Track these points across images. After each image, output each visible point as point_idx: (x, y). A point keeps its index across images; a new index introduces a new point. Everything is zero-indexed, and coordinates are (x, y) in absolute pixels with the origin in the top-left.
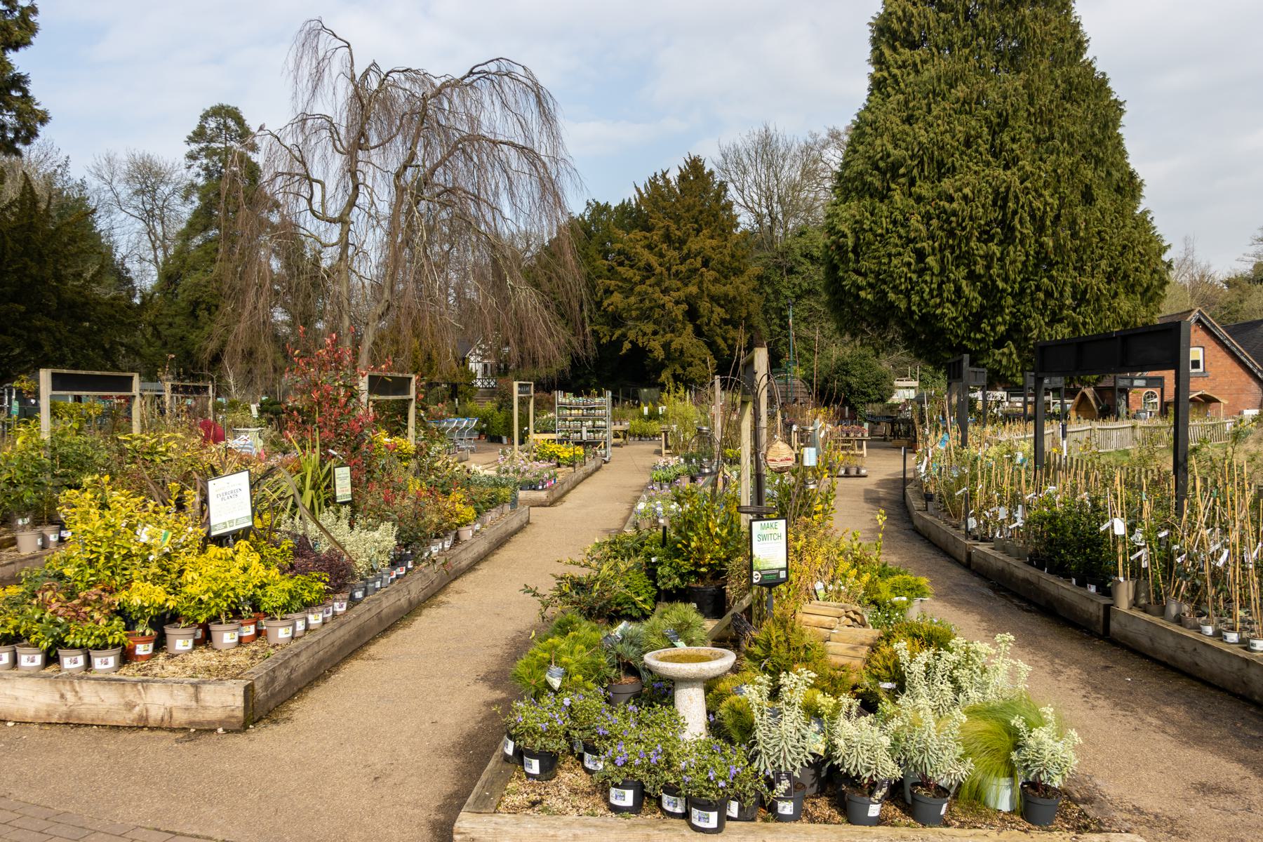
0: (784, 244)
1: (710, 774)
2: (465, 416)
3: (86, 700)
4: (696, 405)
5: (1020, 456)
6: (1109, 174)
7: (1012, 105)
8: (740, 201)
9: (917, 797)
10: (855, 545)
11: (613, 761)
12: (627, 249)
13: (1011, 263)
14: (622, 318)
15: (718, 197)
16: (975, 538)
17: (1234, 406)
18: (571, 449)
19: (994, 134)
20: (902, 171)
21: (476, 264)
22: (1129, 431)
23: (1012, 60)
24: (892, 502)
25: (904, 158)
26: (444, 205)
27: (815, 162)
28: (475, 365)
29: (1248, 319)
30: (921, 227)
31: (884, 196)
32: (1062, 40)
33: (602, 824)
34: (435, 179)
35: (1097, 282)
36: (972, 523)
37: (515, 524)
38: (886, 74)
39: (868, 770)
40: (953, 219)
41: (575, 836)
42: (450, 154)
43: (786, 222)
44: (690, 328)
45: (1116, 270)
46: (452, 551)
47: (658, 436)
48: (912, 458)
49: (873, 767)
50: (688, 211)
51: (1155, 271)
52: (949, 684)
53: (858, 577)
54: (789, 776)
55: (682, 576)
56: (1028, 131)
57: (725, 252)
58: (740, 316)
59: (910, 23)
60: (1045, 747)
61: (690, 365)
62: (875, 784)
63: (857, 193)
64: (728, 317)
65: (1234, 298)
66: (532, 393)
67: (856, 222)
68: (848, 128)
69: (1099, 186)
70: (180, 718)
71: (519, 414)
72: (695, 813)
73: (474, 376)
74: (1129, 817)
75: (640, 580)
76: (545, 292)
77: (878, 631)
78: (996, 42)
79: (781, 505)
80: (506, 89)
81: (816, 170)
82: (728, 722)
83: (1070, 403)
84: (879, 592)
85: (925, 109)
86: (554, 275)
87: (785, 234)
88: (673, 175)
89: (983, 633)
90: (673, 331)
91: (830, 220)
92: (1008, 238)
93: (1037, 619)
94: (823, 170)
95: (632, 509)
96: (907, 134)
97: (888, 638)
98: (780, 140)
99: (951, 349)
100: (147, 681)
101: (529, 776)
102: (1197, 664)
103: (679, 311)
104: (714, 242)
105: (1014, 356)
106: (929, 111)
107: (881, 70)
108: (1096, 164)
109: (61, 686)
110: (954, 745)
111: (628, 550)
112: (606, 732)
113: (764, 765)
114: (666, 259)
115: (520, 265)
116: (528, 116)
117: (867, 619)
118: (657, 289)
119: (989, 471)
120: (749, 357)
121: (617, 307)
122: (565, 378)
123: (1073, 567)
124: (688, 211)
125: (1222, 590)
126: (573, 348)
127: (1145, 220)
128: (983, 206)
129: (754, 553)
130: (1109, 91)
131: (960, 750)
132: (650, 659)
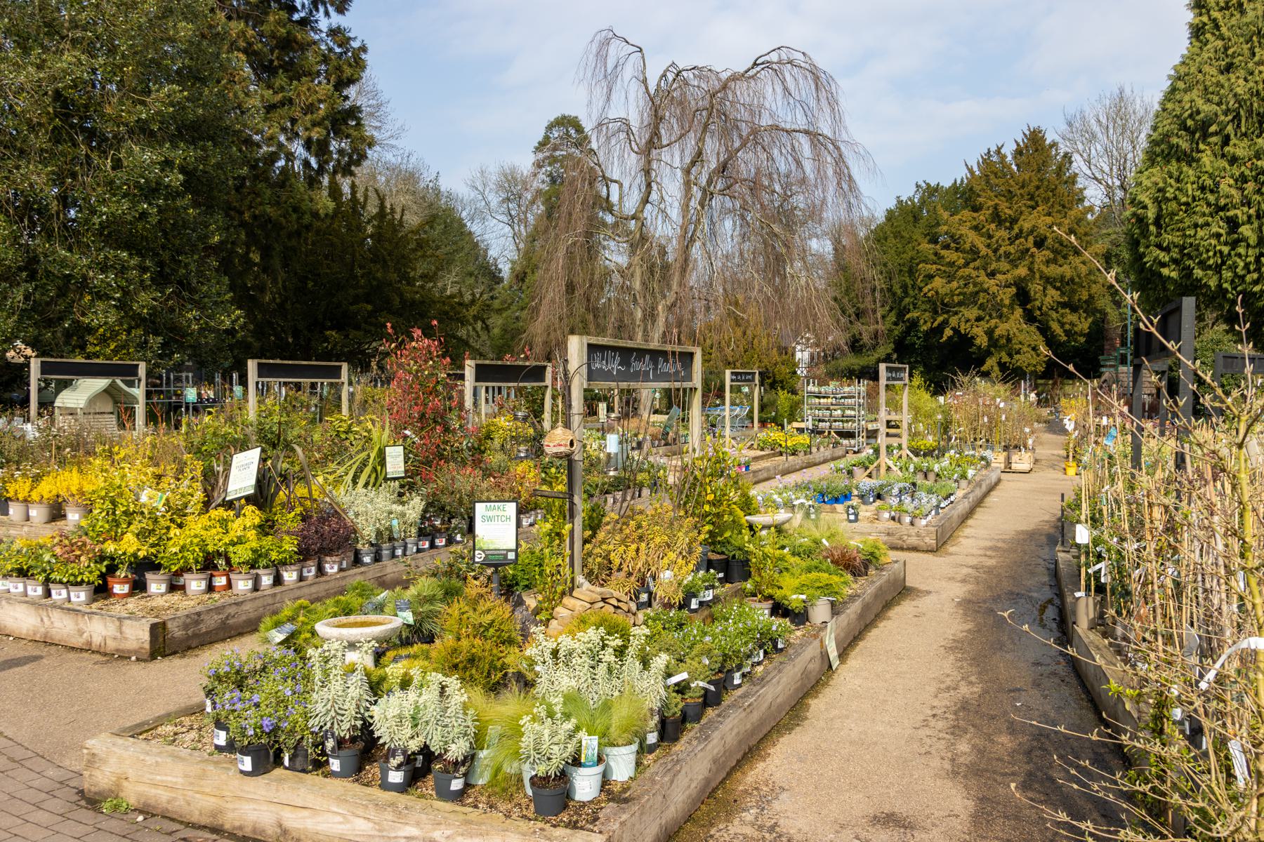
3: (56, 624)
15: (1060, 171)
20: (1213, 129)
25: (1216, 115)
28: (802, 356)
38: (1205, 19)
44: (1019, 312)
50: (1023, 187)
58: (1079, 300)
61: (1018, 352)
67: (1159, 190)
70: (112, 645)
88: (1009, 150)
100: (93, 613)
103: (1006, 295)
107: (1201, 15)
109: (41, 611)
114: (994, 240)
121: (937, 293)
124: (1023, 187)
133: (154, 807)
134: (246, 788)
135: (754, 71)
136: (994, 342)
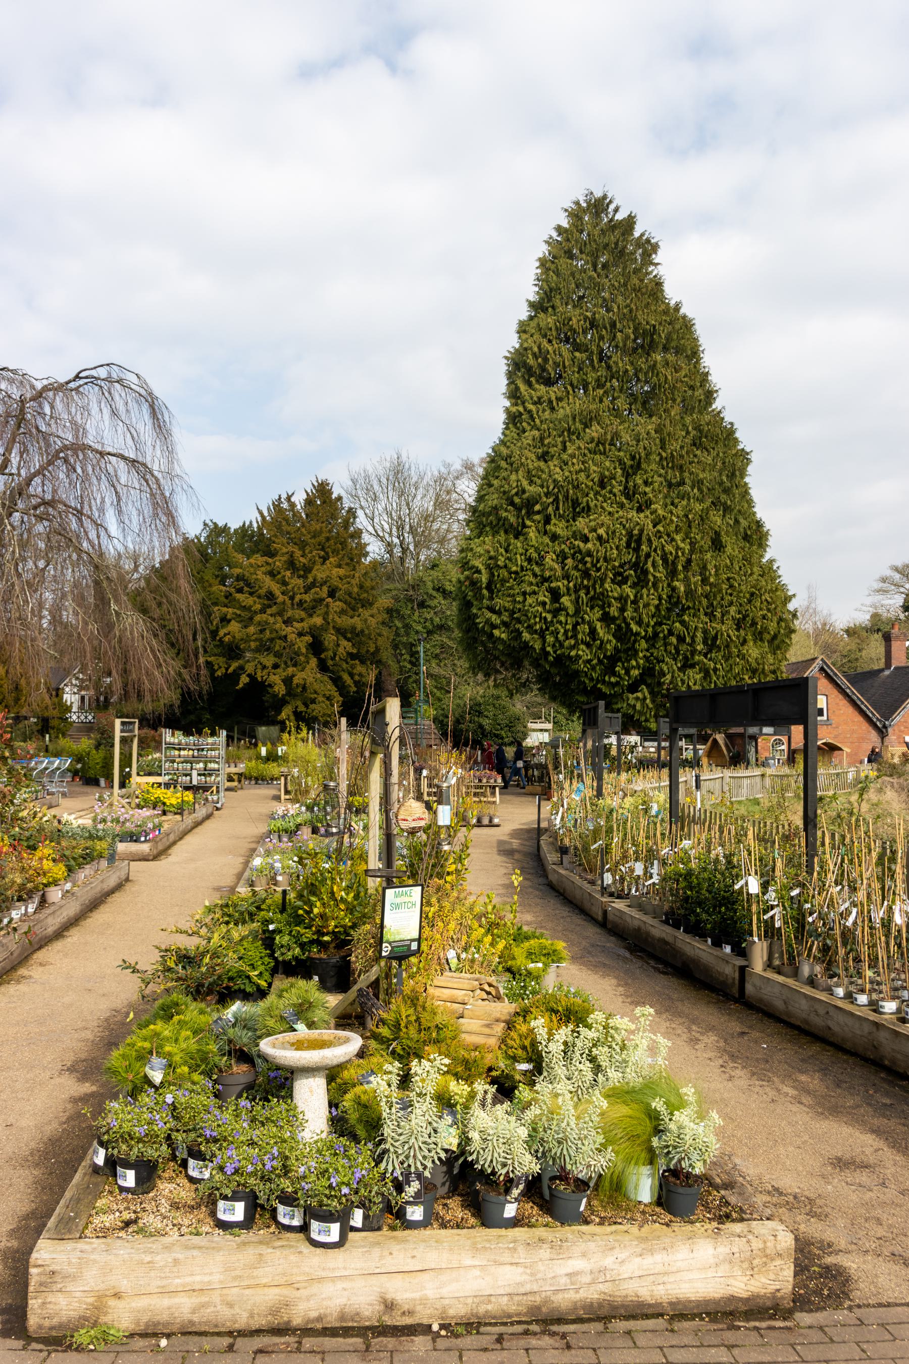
0: (416, 576)
1: (332, 1180)
2: (57, 755)
4: (320, 747)
5: (655, 808)
6: (737, 521)
7: (645, 448)
8: (370, 529)
9: (555, 1193)
10: (490, 908)
11: (221, 1169)
12: (247, 574)
13: (644, 606)
14: (239, 649)
15: (346, 524)
16: (611, 895)
17: (856, 754)
18: (179, 795)
19: (627, 476)
20: (537, 507)
21: (76, 585)
22: (758, 779)
23: (644, 403)
24: (526, 854)
26: (40, 518)
27: (448, 492)
28: (70, 697)
29: (867, 669)
30: (556, 566)
31: (519, 532)
32: (692, 388)
33: (208, 1244)
34: (31, 490)
35: (727, 629)
36: (608, 878)
37: (112, 882)
38: (521, 409)
39: (504, 1165)
40: (588, 559)
41: (176, 1261)
42: (50, 463)
43: (418, 554)
44: (314, 662)
45: (745, 617)
46: (37, 916)
47: (277, 779)
48: (547, 807)
49: (510, 1162)
50: (314, 537)
51: (781, 619)
52: (588, 1064)
53: (492, 944)
54: (419, 1176)
55: (302, 946)
56: (660, 476)
57: (353, 582)
58: (368, 651)
59: (546, 360)
60: (687, 1131)
61: (313, 701)
62: (511, 1181)
63: (492, 528)
64: (355, 651)
65: (854, 647)
66: (136, 732)
67: (491, 558)
68: (482, 460)
69: (727, 533)
71: (121, 754)
72: (315, 1225)
73: (68, 709)
74: (768, 1199)
75: (256, 951)
76: (154, 620)
77: (514, 1005)
78: (629, 385)
79: (412, 865)
80: (117, 397)
81: (449, 501)
82: (353, 1117)
83: (702, 749)
84: (514, 958)
85: (560, 446)
86: (164, 601)
87: (417, 566)
88: (299, 499)
89: (620, 999)
90: (295, 665)
91: (463, 555)
92: (641, 581)
93: (673, 982)
94: (456, 501)
95: (247, 863)
96: (542, 471)
97: (525, 1013)
98: (413, 468)
99: (584, 691)
101: (122, 1189)
102: (830, 1028)
103: (302, 644)
104: (342, 572)
105: (648, 701)
106: (565, 449)
107: (516, 405)
108: (724, 511)
110: (593, 1133)
111: (242, 913)
112: (215, 1134)
113: (392, 1166)
114: (290, 587)
115: (126, 587)
116: (140, 427)
117: (502, 991)
118: (279, 619)
119: (625, 823)
120: (379, 705)
121: (234, 637)
122: (174, 714)
123: (709, 926)
125: (851, 950)
126: (184, 680)
127: (771, 568)
128: (617, 548)
129: (386, 923)
130: (736, 441)
131: (600, 1139)
132: (265, 1046)
133: (167, 1324)
134: (331, 1265)
135: (77, 383)
136: (291, 692)
